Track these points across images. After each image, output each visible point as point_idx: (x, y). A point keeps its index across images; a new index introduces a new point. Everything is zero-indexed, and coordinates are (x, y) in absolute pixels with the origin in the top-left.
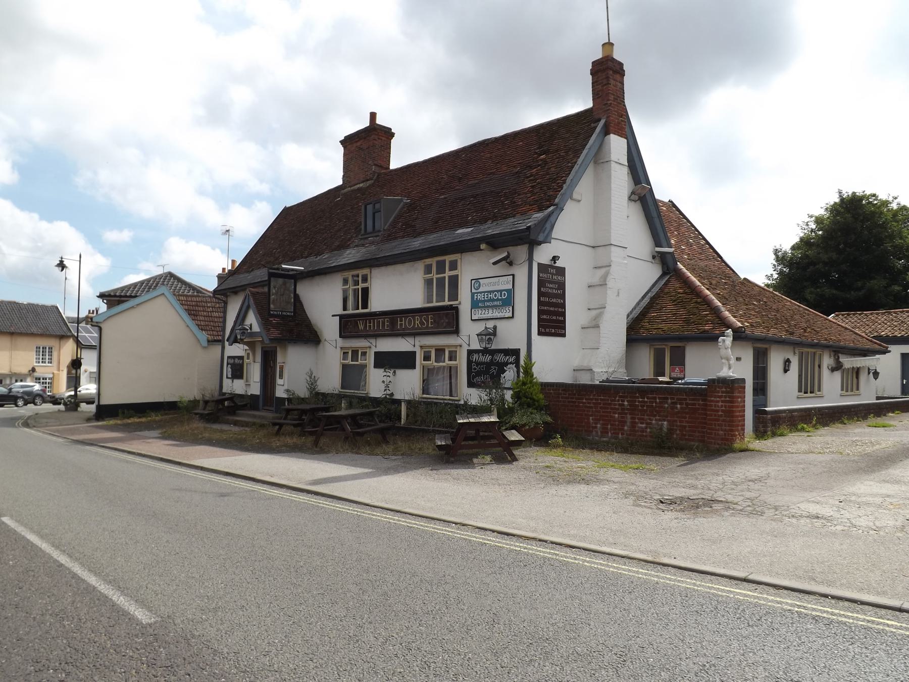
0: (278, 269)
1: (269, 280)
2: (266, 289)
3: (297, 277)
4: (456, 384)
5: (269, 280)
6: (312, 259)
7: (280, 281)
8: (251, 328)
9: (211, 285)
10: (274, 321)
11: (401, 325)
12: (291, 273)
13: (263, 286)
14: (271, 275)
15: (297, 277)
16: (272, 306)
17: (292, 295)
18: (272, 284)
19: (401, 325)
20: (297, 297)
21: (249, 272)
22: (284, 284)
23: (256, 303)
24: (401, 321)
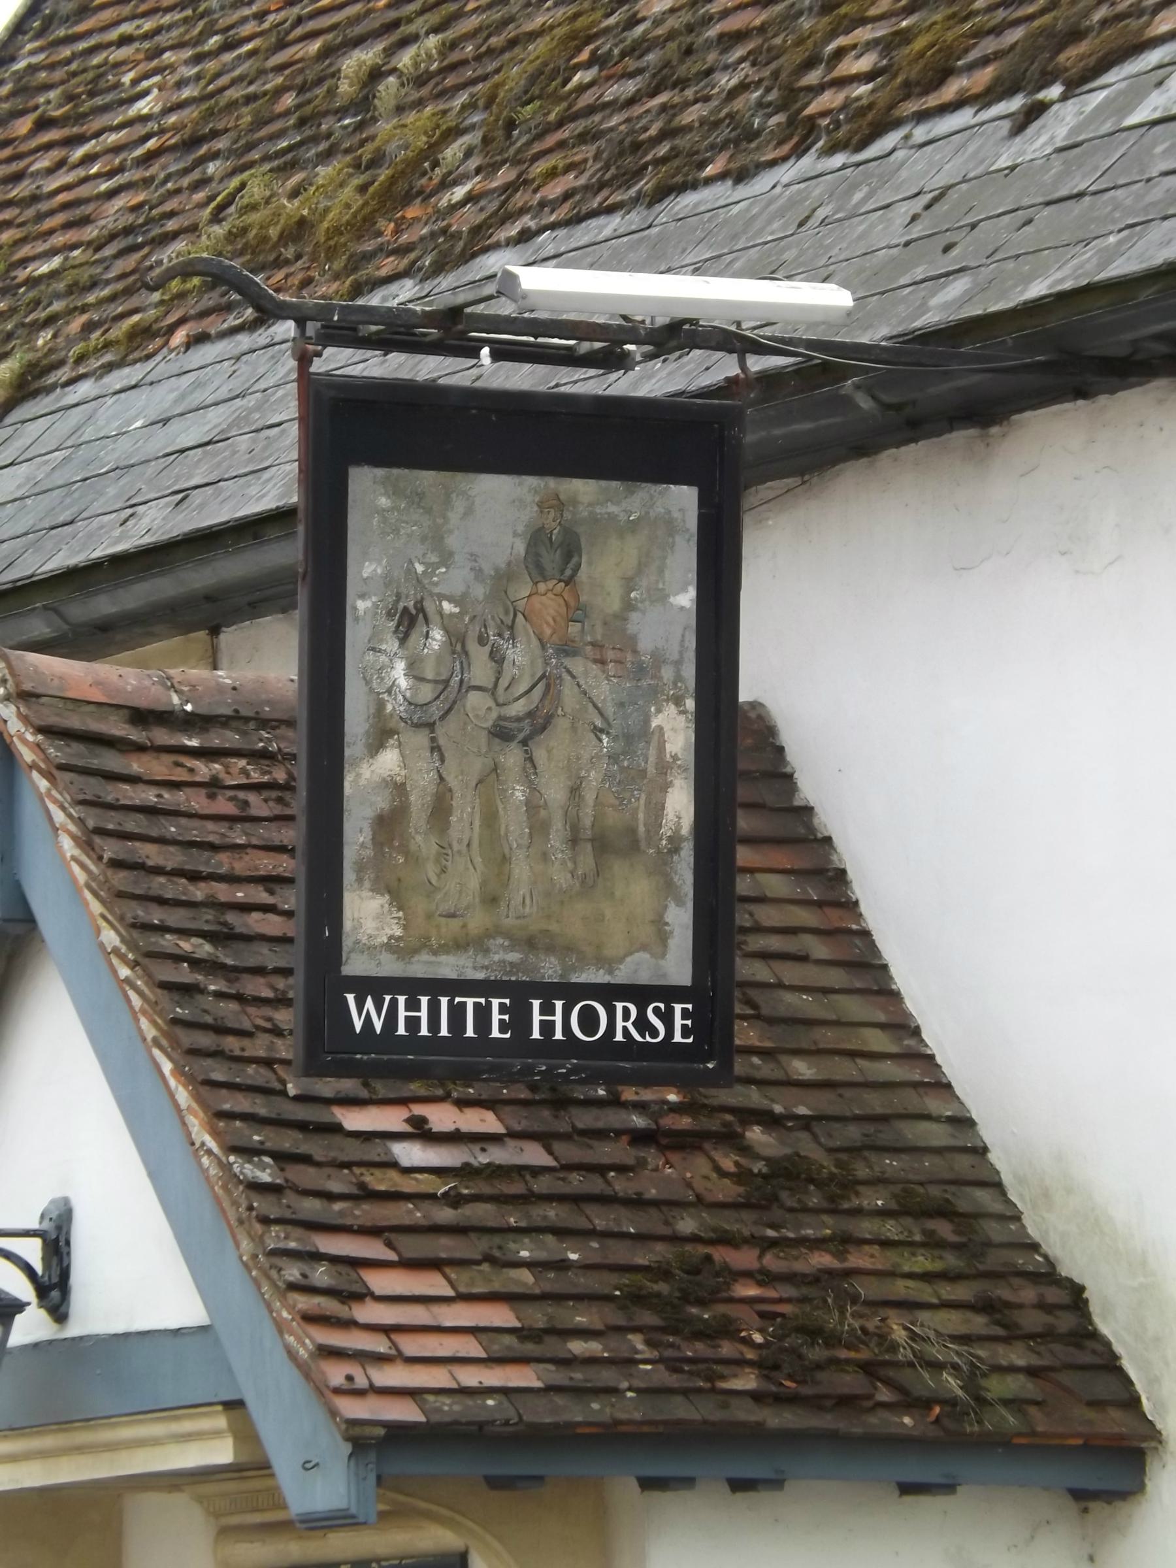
0: (452, 332)
1: (323, 515)
2: (266, 661)
3: (739, 443)
4: (152, 1419)
5: (323, 515)
6: (955, 146)
7: (496, 508)
8: (54, 1288)
9: (735, 355)
10: (420, 1141)
11: (547, 1027)
12: (652, 380)
13: (211, 616)
14: (349, 430)
15: (739, 443)
16: (367, 916)
17: (676, 730)
18: (367, 570)
19: (547, 1027)
20: (740, 758)
21: (741, 176)
22: (556, 552)
23: (135, 890)
24: (547, 1009)
